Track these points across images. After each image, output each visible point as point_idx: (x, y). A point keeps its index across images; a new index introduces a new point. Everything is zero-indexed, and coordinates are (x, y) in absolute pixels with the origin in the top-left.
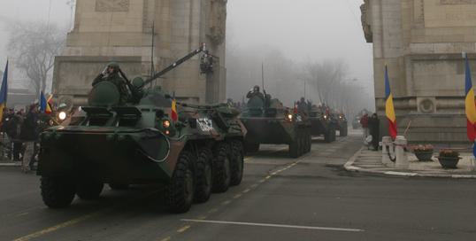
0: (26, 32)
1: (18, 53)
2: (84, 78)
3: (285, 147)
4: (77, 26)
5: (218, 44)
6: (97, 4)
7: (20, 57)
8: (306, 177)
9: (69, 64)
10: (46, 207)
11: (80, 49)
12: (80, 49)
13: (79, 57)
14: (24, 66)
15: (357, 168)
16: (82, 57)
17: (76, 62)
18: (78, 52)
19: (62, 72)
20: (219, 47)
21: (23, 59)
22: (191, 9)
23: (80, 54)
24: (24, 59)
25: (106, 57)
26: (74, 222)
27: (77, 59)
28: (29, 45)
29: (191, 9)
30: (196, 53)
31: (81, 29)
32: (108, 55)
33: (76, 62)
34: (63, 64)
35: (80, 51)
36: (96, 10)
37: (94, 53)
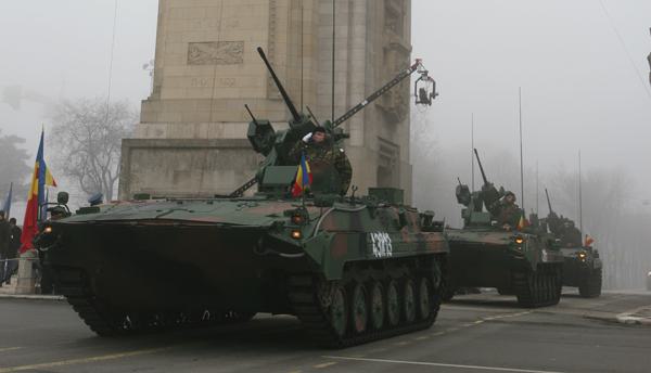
0: (78, 116)
1: (66, 151)
2: (171, 174)
3: (515, 299)
4: (157, 89)
5: (398, 122)
6: (189, 52)
7: (69, 159)
8: (548, 324)
9: (145, 152)
10: (94, 334)
11: (163, 127)
12: (163, 127)
13: (163, 140)
14: (75, 173)
15: (638, 319)
16: (168, 140)
17: (156, 148)
18: (159, 132)
19: (135, 166)
20: (399, 126)
21: (74, 162)
22: (349, 61)
23: (164, 136)
24: (76, 161)
25: (207, 140)
26: (148, 352)
27: (159, 144)
28: (84, 139)
29: (349, 61)
30: (359, 107)
31: (165, 95)
32: (211, 137)
33: (156, 148)
34: (136, 153)
35: (164, 130)
36: (190, 62)
37: (187, 133)
